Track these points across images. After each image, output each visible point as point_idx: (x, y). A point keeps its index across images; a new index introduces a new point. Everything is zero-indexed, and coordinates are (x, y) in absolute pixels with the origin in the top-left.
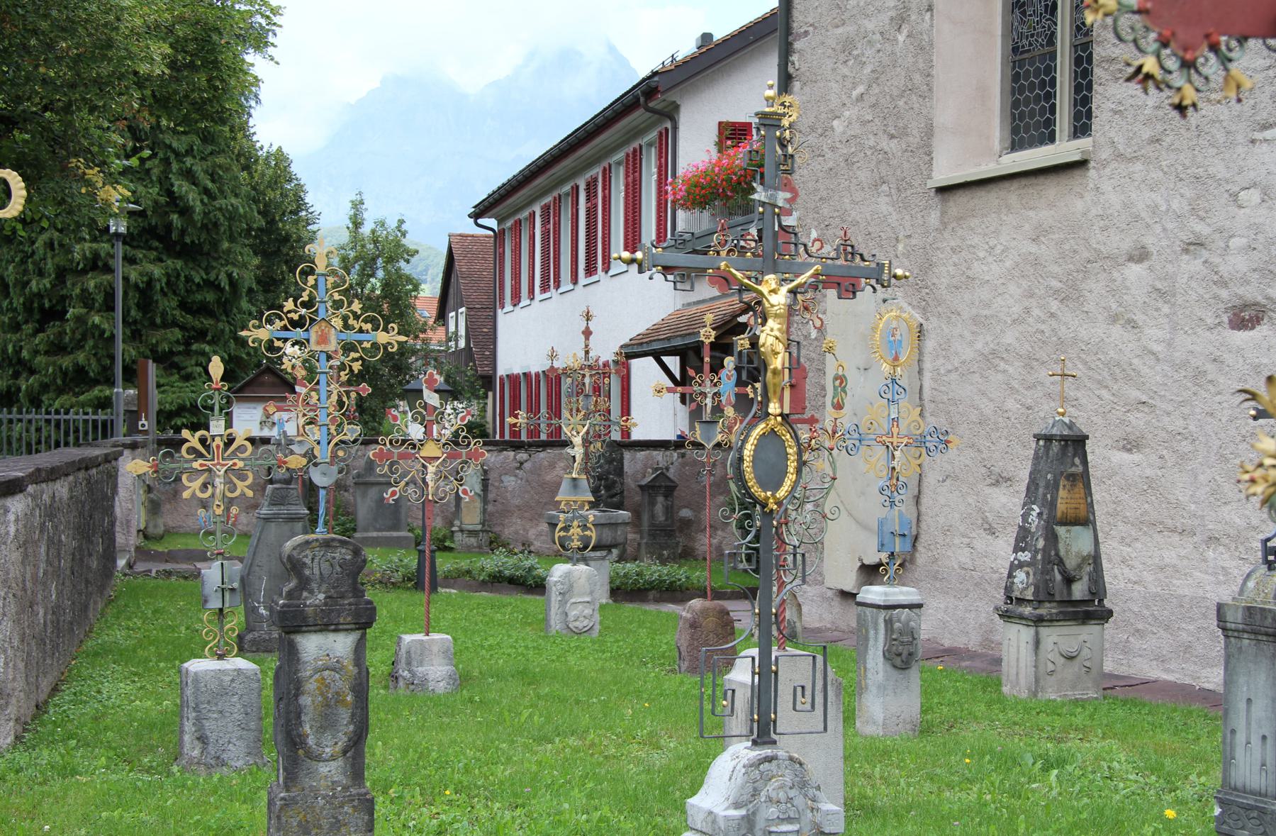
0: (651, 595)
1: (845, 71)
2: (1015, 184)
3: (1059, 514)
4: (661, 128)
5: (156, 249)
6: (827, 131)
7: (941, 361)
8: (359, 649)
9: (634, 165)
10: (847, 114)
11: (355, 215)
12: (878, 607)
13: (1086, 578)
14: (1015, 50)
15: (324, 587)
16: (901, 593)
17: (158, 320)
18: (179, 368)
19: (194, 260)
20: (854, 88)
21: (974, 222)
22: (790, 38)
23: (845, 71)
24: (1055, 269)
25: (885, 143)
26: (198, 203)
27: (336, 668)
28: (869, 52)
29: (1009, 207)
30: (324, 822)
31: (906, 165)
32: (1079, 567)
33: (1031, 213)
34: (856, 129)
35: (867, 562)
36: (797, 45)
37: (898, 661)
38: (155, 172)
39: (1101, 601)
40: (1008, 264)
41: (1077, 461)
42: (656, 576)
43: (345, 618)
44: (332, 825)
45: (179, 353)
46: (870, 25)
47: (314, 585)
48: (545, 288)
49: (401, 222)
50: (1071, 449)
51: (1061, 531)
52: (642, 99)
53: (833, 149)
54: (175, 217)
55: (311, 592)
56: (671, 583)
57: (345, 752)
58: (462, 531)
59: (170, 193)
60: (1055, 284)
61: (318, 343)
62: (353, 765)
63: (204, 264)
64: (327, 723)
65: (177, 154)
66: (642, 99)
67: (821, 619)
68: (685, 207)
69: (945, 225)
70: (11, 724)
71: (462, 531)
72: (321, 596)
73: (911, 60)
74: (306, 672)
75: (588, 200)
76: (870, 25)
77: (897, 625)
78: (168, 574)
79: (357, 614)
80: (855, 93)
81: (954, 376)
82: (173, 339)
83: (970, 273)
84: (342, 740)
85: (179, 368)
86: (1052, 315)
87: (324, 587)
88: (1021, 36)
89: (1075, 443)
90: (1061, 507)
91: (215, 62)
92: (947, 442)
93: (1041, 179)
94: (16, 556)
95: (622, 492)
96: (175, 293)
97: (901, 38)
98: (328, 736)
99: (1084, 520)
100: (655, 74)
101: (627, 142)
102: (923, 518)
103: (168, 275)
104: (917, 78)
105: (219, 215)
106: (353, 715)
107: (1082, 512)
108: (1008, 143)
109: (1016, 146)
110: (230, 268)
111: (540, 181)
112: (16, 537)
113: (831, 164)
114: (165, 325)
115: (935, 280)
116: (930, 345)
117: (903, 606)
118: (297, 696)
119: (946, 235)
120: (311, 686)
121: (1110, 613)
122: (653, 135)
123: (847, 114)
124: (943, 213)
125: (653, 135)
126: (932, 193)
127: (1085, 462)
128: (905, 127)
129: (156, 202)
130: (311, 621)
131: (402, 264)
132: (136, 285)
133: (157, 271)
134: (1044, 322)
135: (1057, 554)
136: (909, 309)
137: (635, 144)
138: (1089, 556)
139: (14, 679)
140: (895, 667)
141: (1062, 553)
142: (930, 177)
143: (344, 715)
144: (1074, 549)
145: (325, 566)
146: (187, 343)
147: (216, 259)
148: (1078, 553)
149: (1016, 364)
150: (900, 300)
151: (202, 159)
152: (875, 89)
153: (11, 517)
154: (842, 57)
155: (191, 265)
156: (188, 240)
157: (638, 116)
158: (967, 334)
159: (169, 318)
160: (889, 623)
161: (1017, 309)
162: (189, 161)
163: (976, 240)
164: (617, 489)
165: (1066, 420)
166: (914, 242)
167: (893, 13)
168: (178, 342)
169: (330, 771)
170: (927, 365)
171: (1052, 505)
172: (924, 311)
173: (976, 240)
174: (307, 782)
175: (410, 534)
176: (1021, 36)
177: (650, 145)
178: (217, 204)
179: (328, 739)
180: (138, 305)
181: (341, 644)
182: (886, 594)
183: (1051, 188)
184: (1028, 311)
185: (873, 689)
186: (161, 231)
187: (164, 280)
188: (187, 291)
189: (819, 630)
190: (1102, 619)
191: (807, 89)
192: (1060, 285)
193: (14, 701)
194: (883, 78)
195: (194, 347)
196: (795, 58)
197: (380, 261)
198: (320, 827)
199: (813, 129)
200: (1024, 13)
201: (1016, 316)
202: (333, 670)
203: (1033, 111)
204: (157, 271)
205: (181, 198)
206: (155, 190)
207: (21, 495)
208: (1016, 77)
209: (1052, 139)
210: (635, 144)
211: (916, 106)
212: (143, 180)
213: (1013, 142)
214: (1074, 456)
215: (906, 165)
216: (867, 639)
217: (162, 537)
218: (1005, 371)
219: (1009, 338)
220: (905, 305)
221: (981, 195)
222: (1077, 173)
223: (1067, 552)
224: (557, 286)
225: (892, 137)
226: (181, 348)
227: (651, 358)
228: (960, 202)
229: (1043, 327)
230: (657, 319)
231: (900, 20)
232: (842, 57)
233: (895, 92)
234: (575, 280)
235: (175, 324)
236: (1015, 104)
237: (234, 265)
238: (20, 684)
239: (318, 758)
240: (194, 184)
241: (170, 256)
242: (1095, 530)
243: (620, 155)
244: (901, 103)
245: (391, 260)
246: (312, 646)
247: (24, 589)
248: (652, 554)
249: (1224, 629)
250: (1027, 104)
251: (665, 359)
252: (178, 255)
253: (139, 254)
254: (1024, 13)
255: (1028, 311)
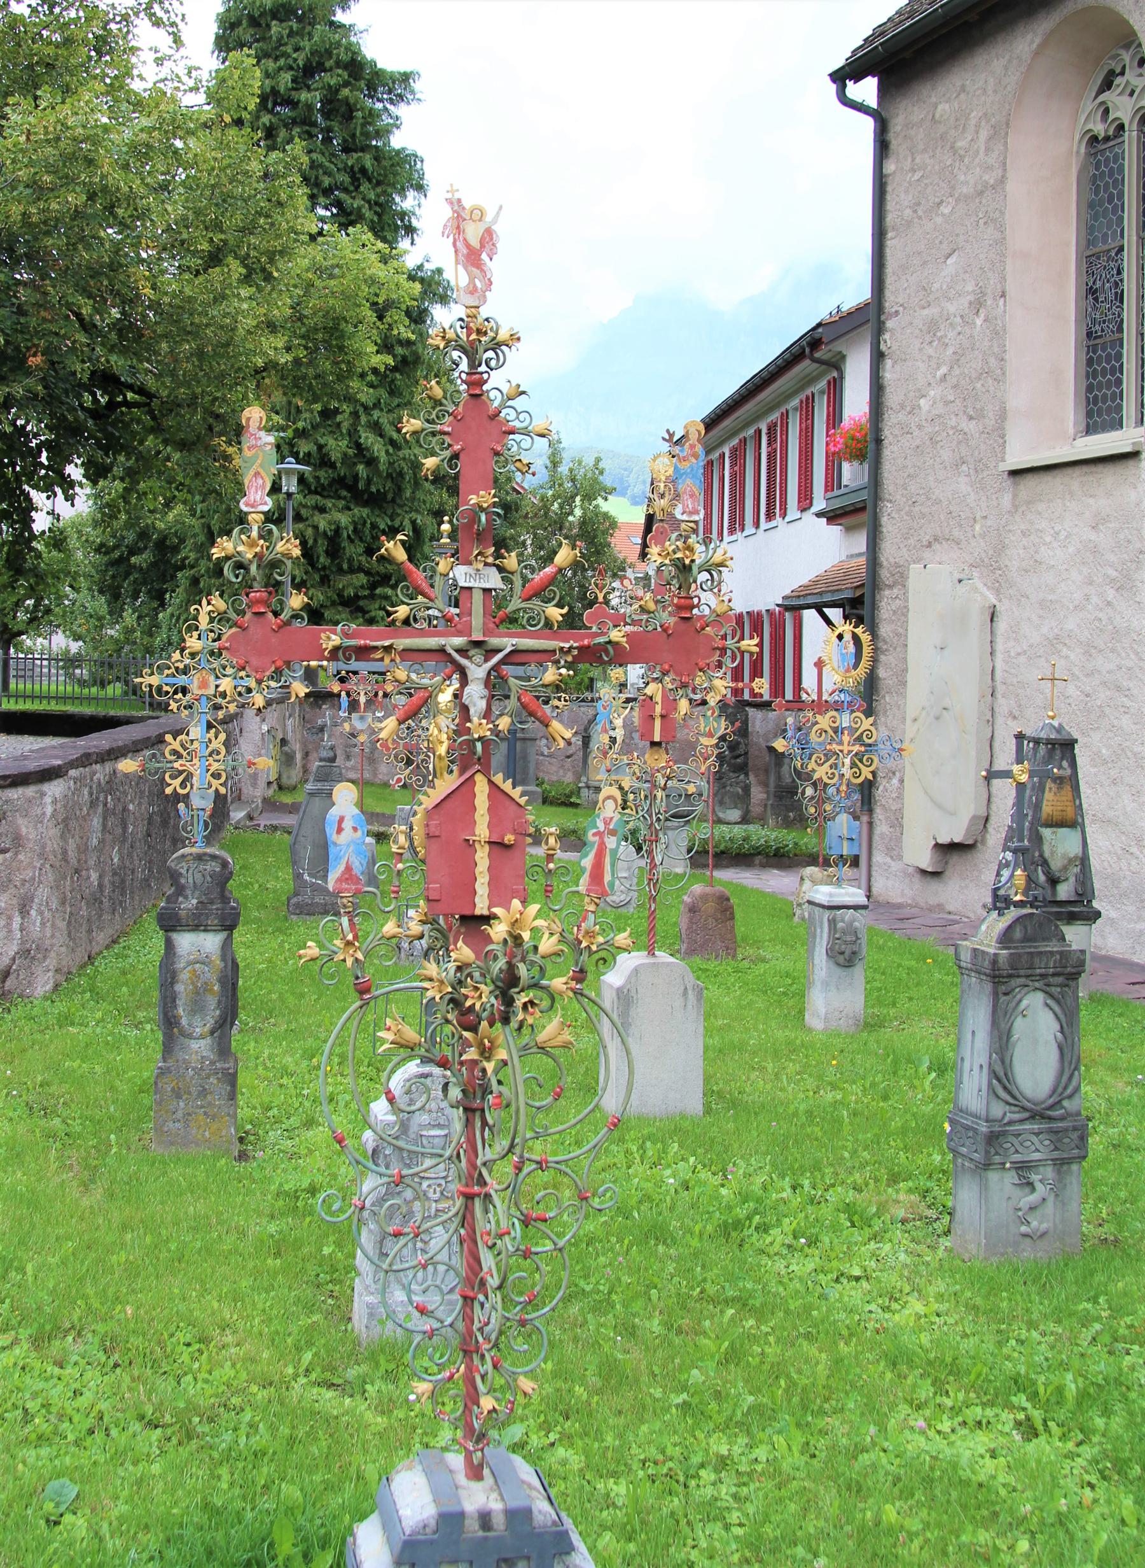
0: (757, 860)
1: (930, 351)
2: (1077, 471)
3: (1044, 815)
4: (829, 377)
5: (344, 498)
6: (914, 410)
7: (1012, 643)
8: (227, 945)
9: (807, 410)
10: (932, 393)
11: (553, 454)
12: (823, 907)
13: (1072, 880)
14: (1089, 335)
15: (197, 893)
16: (847, 894)
17: (345, 566)
18: (364, 612)
19: (380, 508)
20: (938, 368)
21: (1041, 507)
22: (883, 318)
23: (930, 351)
24: (1112, 558)
25: (965, 425)
26: (383, 453)
27: (206, 962)
28: (951, 334)
29: (1071, 494)
30: (193, 1089)
31: (983, 447)
32: (1065, 868)
33: (1091, 501)
34: (940, 409)
35: (940, 841)
36: (889, 324)
37: (841, 959)
38: (345, 426)
39: (1090, 901)
40: (1071, 550)
41: (1065, 764)
42: (762, 841)
43: (213, 921)
44: (200, 1093)
45: (365, 597)
46: (951, 308)
47: (189, 892)
48: (732, 531)
49: (598, 460)
50: (1058, 752)
51: (1046, 832)
52: (807, 350)
53: (920, 427)
54: (361, 468)
55: (186, 897)
56: (778, 849)
57: (212, 1033)
58: (588, 787)
59: (358, 446)
60: (1112, 573)
61: (200, 688)
62: (219, 1044)
63: (389, 512)
64: (197, 1007)
65: (366, 408)
66: (807, 350)
67: (903, 895)
68: (846, 459)
69: (1016, 507)
70: (50, 974)
71: (588, 787)
72: (194, 901)
73: (987, 343)
74: (180, 964)
75: (769, 444)
76: (951, 308)
77: (840, 925)
78: (275, 828)
79: (223, 918)
80: (939, 373)
81: (1022, 659)
82: (359, 584)
83: (1037, 557)
84: (210, 1022)
85: (364, 612)
86: (1109, 604)
87: (197, 893)
88: (1094, 321)
89: (1064, 747)
90: (1047, 809)
91: (341, 348)
92: (901, 750)
93: (1100, 468)
94: (55, 832)
95: (746, 753)
96: (361, 540)
97: (979, 322)
98: (198, 1018)
99: (1072, 822)
100: (819, 325)
101: (802, 388)
102: (993, 799)
103: (354, 523)
104: (992, 361)
105: (403, 464)
106: (219, 1002)
107: (1070, 813)
108: (1083, 426)
109: (1090, 430)
110: (414, 515)
111: (727, 423)
112: (53, 815)
113: (918, 442)
114: (352, 571)
115: (1007, 562)
116: (1002, 625)
117: (848, 907)
118: (172, 984)
119: (1017, 518)
120: (184, 976)
121: (1098, 914)
122: (823, 384)
123: (932, 393)
124: (1015, 496)
125: (823, 384)
126: (1006, 475)
127: (1073, 764)
128: (982, 409)
129: (345, 454)
130: (184, 922)
131: (600, 501)
132: (325, 533)
133: (344, 519)
134: (1101, 610)
135: (1041, 855)
136: (984, 590)
137: (808, 392)
138: (1076, 857)
139: (53, 936)
140: (838, 964)
141: (1047, 854)
142: (1003, 460)
143: (212, 1002)
144: (1060, 851)
145: (198, 876)
146: (373, 586)
147: (401, 506)
148: (1064, 855)
149: (1078, 650)
150: (976, 580)
151: (389, 411)
152: (956, 371)
153: (48, 800)
154: (928, 338)
155: (377, 512)
156: (374, 489)
157: (805, 366)
158: (1034, 618)
159: (356, 563)
160: (832, 922)
161: (1078, 596)
162: (376, 414)
163: (1043, 524)
164: (741, 751)
165: (1055, 723)
166: (989, 523)
167: (971, 298)
168: (362, 587)
169: (200, 1047)
170: (999, 647)
171: (1037, 807)
172: (998, 592)
173: (1043, 524)
174: (181, 1055)
175: (538, 789)
176: (1094, 321)
177: (822, 392)
178: (401, 454)
179: (197, 1021)
180: (327, 552)
181: (210, 942)
182: (831, 895)
183: (1109, 475)
184: (1087, 598)
185: (818, 984)
186: (349, 481)
187: (351, 528)
188: (373, 537)
189: (899, 906)
190: (1088, 919)
191: (898, 368)
192: (1115, 574)
193: (53, 954)
194: (963, 360)
195: (378, 591)
196: (887, 336)
197: (578, 499)
198: (189, 1093)
199: (902, 406)
200: (1096, 299)
201: (1076, 603)
202: (203, 963)
203: (1105, 396)
204: (344, 519)
205: (368, 449)
206: (344, 443)
207: (61, 780)
208: (1090, 362)
209: (1118, 424)
210: (808, 392)
211: (991, 389)
212: (334, 433)
213: (1088, 425)
214: (1062, 759)
215: (983, 447)
216: (814, 936)
217: (295, 788)
218: (1067, 657)
219: (1071, 624)
220: (980, 586)
221: (1047, 479)
222: (1131, 463)
223: (1052, 853)
224: (784, 515)
225: (971, 418)
226: (366, 593)
227: (813, 611)
228: (1030, 481)
229: (1100, 615)
230: (820, 570)
231: (977, 305)
232: (928, 338)
233: (974, 375)
234: (757, 525)
235: (360, 569)
236: (1090, 389)
237: (417, 511)
238: (61, 938)
239: (190, 1036)
240: (381, 436)
241: (357, 504)
242: (1083, 833)
243: (795, 402)
244: (979, 385)
245: (589, 497)
246: (186, 942)
247: (65, 859)
248: (778, 815)
249: (960, 967)
250: (1100, 389)
251: (826, 610)
252: (365, 504)
253: (329, 504)
254: (1096, 299)
255: (1087, 598)
